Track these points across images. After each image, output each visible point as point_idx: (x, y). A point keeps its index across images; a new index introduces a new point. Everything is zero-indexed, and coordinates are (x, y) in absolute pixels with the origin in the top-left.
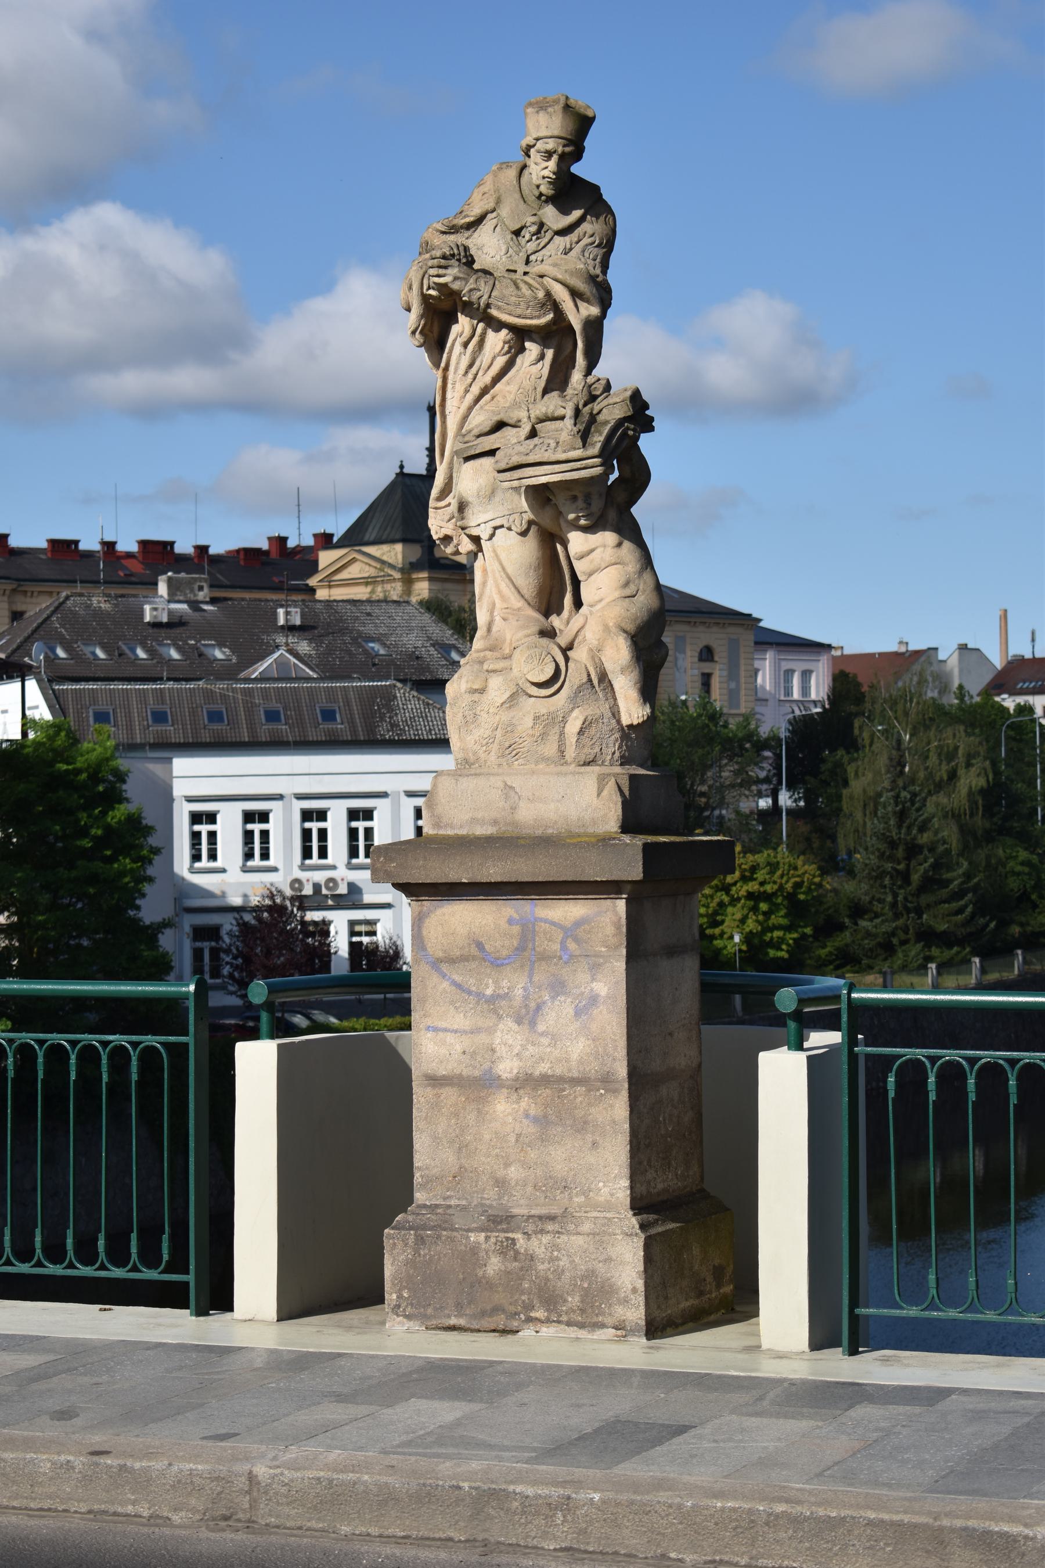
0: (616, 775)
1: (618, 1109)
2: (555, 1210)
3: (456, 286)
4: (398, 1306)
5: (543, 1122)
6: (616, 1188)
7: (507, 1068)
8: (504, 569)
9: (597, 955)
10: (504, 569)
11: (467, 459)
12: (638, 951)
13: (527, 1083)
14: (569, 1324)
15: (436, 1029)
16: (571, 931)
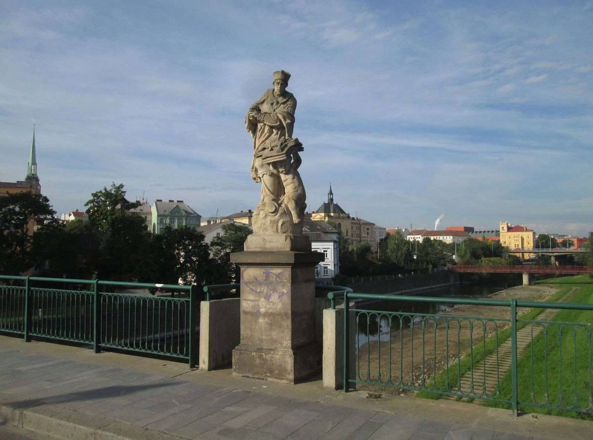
0: (290, 236)
1: (288, 323)
2: (272, 348)
3: (255, 116)
4: (235, 370)
5: (271, 325)
6: (287, 342)
7: (263, 310)
8: (266, 186)
9: (284, 282)
10: (266, 186)
11: (258, 157)
12: (294, 280)
13: (267, 315)
14: (275, 378)
15: (246, 300)
16: (278, 276)
